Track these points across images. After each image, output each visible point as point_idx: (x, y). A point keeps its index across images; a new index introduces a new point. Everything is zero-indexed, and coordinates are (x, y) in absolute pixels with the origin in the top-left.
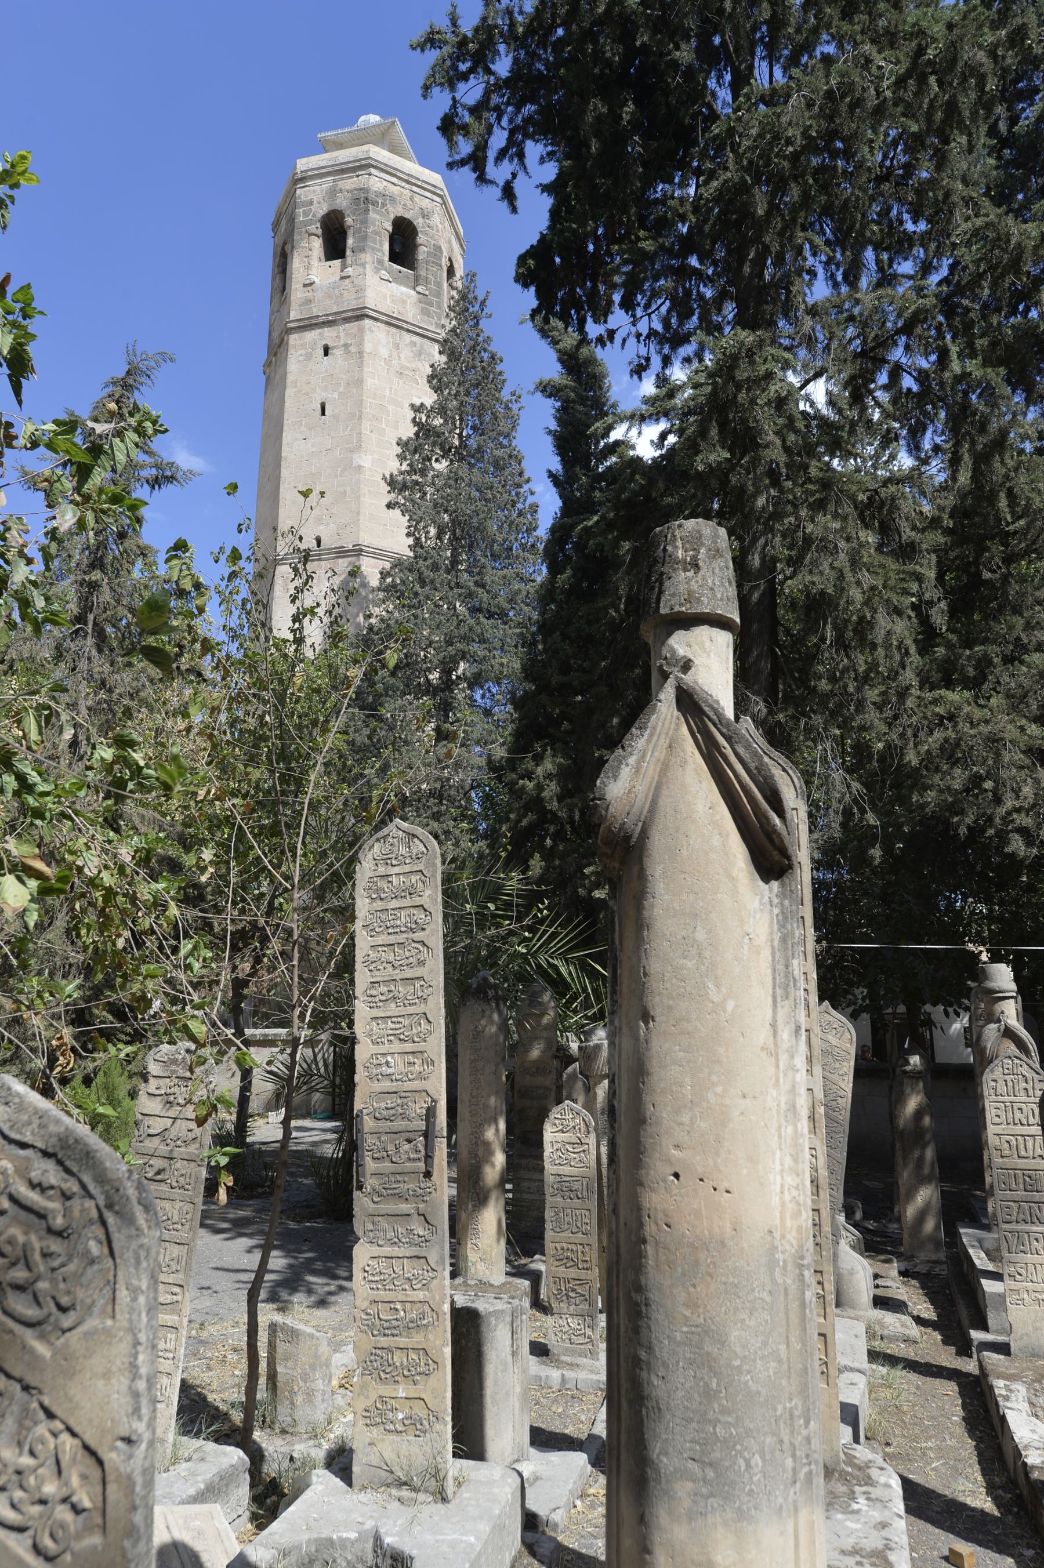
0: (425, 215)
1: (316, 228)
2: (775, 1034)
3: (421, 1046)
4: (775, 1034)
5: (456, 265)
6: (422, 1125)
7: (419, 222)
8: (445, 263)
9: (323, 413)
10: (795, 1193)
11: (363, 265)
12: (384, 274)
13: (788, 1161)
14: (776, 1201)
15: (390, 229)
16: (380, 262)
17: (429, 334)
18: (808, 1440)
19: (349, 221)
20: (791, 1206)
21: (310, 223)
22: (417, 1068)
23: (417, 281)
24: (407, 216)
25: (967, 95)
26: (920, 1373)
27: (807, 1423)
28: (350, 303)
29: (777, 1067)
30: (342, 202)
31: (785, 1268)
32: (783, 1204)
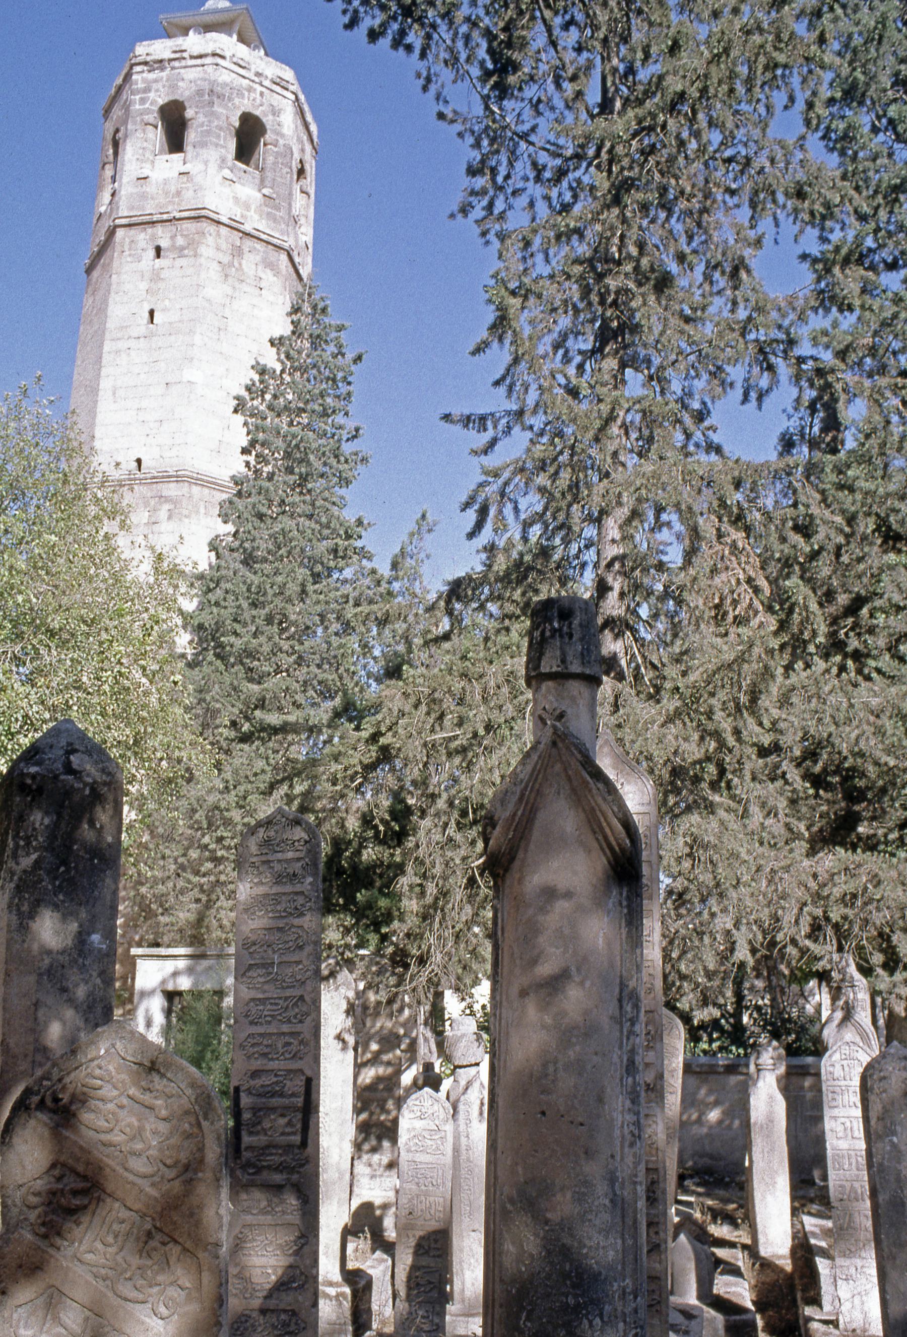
0: (276, 112)
1: (153, 117)
2: (621, 1007)
3: (298, 1028)
4: (621, 1007)
5: (307, 167)
6: (300, 1101)
7: (268, 120)
8: (295, 165)
9: (152, 313)
10: (632, 1128)
11: (206, 163)
12: (227, 173)
13: (628, 1103)
14: (617, 1132)
15: (237, 124)
16: (223, 160)
17: (275, 241)
18: (636, 1311)
19: (189, 113)
20: (628, 1137)
21: (148, 111)
22: (294, 1048)
23: (262, 184)
24: (257, 112)
25: (707, 1095)
26: (818, 1105)
27: (636, 1297)
28: (190, 200)
29: (621, 1032)
30: (184, 92)
31: (623, 1183)
32: (623, 1137)
